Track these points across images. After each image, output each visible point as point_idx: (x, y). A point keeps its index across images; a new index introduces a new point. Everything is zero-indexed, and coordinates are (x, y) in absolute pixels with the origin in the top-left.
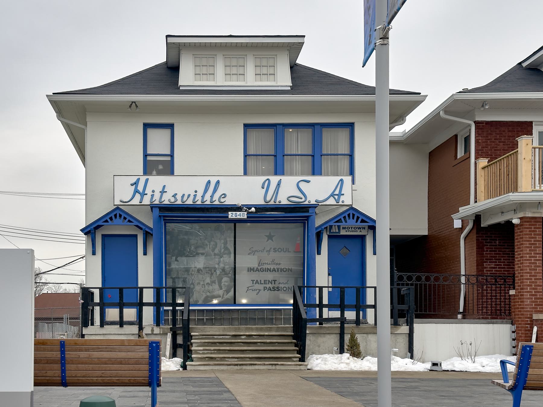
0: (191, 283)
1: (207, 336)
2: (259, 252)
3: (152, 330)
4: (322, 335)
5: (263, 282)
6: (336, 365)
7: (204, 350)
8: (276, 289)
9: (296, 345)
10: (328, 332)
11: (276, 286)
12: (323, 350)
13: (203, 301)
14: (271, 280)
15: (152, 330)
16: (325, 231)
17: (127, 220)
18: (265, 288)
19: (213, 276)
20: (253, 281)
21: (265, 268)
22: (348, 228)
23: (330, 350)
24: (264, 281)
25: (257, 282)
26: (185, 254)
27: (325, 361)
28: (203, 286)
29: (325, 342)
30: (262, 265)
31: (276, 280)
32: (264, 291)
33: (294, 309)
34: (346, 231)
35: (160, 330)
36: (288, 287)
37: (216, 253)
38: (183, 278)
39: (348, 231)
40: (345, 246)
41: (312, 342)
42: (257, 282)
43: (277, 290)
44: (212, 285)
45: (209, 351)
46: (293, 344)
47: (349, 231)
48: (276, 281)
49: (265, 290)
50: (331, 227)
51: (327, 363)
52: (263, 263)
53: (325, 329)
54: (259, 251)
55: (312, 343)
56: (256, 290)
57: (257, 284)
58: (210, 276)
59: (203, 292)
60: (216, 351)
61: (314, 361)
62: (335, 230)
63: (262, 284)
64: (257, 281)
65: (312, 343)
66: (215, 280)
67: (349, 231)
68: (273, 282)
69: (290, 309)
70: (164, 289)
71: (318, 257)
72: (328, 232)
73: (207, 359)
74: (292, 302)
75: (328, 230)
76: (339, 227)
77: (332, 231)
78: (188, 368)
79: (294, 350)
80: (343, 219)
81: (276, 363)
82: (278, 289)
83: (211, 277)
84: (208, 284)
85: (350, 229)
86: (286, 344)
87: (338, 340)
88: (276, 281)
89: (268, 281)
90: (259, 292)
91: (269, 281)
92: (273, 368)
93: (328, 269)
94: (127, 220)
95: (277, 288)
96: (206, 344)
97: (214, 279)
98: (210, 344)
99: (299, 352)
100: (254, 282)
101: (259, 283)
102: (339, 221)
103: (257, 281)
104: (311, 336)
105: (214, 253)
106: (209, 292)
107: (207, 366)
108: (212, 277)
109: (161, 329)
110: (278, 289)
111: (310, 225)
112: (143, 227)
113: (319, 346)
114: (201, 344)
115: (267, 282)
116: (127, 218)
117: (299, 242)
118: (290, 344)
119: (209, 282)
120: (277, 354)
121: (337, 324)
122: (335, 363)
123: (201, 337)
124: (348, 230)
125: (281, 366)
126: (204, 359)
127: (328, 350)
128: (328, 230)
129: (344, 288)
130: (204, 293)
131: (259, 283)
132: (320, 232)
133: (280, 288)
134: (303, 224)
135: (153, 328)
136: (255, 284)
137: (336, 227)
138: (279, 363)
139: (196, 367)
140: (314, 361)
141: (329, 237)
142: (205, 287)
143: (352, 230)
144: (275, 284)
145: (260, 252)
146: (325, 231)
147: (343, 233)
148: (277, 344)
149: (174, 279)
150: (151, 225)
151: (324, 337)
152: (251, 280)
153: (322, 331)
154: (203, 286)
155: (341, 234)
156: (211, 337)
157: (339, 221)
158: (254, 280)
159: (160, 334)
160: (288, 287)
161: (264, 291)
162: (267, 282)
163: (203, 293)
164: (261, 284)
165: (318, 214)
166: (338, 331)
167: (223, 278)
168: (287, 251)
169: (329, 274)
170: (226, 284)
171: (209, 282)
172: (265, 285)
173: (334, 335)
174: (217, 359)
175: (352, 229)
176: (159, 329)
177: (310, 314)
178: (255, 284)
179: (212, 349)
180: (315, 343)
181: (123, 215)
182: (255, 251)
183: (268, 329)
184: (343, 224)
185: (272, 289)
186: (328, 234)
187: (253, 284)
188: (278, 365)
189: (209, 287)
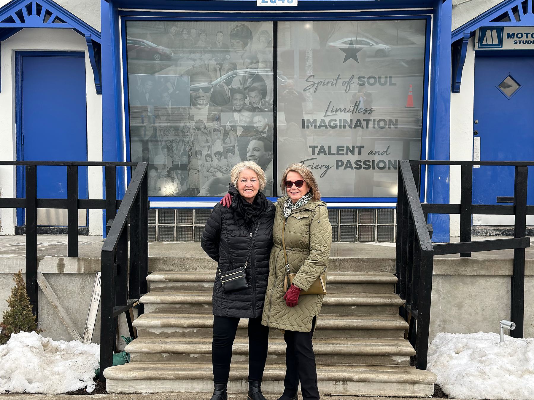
0: (182, 151)
1: (186, 284)
2: (327, 84)
3: (61, 265)
4: (468, 280)
5: (334, 150)
6: (513, 378)
7: (164, 326)
8: (363, 166)
9: (403, 313)
10: (483, 272)
11: (363, 158)
12: (470, 315)
13: (209, 191)
14: (353, 147)
15: (61, 265)
16: (469, 42)
17: (53, 17)
18: (340, 164)
19: (230, 138)
20: (313, 147)
21: (340, 120)
22: (520, 36)
23: (488, 317)
24: (338, 147)
25: (322, 150)
26: (169, 89)
27: (481, 362)
28: (209, 159)
29: (476, 295)
30: (334, 113)
31: (363, 147)
32: (337, 168)
33: (398, 208)
34: (515, 42)
35: (79, 265)
36: (389, 161)
37: (234, 87)
38: (166, 141)
39: (520, 41)
40: (510, 76)
41: (443, 295)
42: (322, 150)
43: (364, 168)
44: (226, 157)
45: (178, 330)
46: (394, 308)
47: (522, 42)
48: (362, 149)
49: (339, 168)
50: (483, 30)
51: (487, 369)
52: (335, 109)
53: (475, 265)
54: (326, 82)
55: (443, 299)
56: (320, 168)
57: (322, 155)
58: (222, 137)
59: (208, 172)
60: (195, 330)
61: (451, 357)
62: (491, 39)
63: (334, 154)
64: (322, 147)
65: (443, 299)
66: (234, 147)
67: (522, 42)
68: (356, 150)
69: (392, 208)
70: (125, 167)
71: (453, 97)
72: (476, 45)
73: (165, 355)
74: (394, 191)
75: (477, 40)
76: (500, 30)
77: (484, 42)
78: (110, 386)
79: (398, 329)
80: (511, 14)
81: (346, 375)
82: (367, 165)
83: (224, 140)
84: (218, 153)
85: (524, 39)
86: (379, 308)
87: (508, 291)
88: (362, 149)
89: (345, 149)
90: (326, 171)
91: (347, 147)
92: (338, 389)
93: (474, 122)
94: (53, 17)
95: (361, 166)
96: (177, 306)
97: (231, 145)
98: (186, 306)
99: (410, 336)
100: (317, 150)
101: (327, 153)
102: (504, 17)
103: (322, 147)
104: (440, 281)
105: (230, 87)
106: (221, 172)
107: (158, 382)
108: (227, 140)
109: (82, 263)
110: (367, 165)
111: (440, 21)
112: (87, 33)
113: (460, 306)
114: (163, 305)
115: (343, 150)
116: (52, 13)
117: (411, 94)
118: (387, 308)
119: (221, 150)
120: (350, 343)
121: (490, 235)
122: (510, 373)
123: (170, 285)
124: (520, 39)
125: (361, 383)
126: (158, 355)
127: (483, 315)
128: (477, 40)
129: (524, 165)
130: (211, 172)
131: (327, 153)
132: (461, 41)
133: (371, 164)
134: (425, 21)
135: (61, 260)
136: (318, 154)
137: (495, 32)
138: (356, 376)
139: (129, 383)
140: (451, 357)
141: (479, 55)
142: (212, 161)
143: (527, 40)
144: (360, 154)
145: (330, 85)
146: (469, 42)
147: (508, 45)
148: (353, 307)
149: (145, 144)
150: (97, 25)
151: (473, 284)
152: (310, 147)
153: (468, 270)
154: (209, 159)
155: (504, 48)
156: (196, 284)
157: (504, 17)
158: (317, 147)
159: (79, 274)
160: (389, 161)
161: (337, 168)
162: (343, 150)
163: (209, 173)
164: (330, 154)
165: (456, 6)
166: (508, 270)
167: (249, 142)
168: (388, 84)
169: (475, 134)
170: (257, 154)
171: (221, 150)
172: (340, 158)
173: (497, 279)
174: (192, 356)
175: (527, 37)
176: (77, 263)
177: (436, 218)
178: (318, 154)
179: (185, 326)
180: (450, 299)
181: (55, 13)
182: (318, 83)
183: (337, 263)
184: (509, 27)
185: (354, 166)
186: (476, 48)
187: (313, 153)
188: (351, 380)
189: (220, 160)
